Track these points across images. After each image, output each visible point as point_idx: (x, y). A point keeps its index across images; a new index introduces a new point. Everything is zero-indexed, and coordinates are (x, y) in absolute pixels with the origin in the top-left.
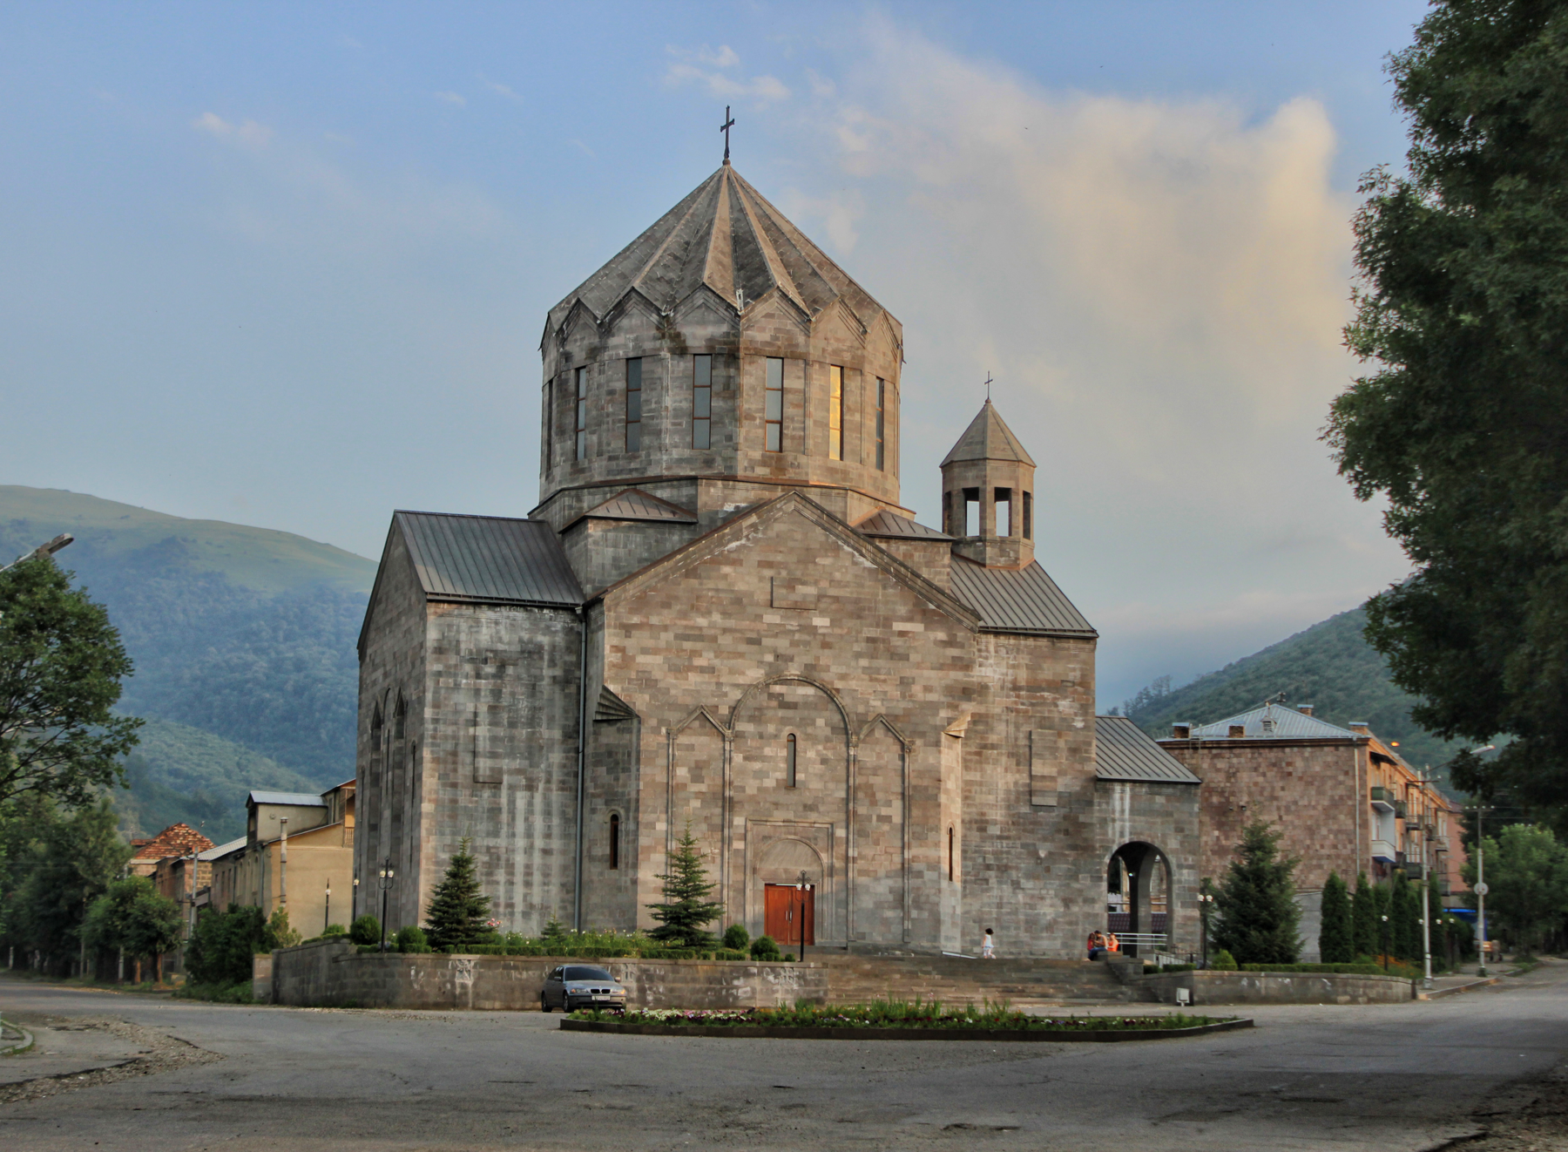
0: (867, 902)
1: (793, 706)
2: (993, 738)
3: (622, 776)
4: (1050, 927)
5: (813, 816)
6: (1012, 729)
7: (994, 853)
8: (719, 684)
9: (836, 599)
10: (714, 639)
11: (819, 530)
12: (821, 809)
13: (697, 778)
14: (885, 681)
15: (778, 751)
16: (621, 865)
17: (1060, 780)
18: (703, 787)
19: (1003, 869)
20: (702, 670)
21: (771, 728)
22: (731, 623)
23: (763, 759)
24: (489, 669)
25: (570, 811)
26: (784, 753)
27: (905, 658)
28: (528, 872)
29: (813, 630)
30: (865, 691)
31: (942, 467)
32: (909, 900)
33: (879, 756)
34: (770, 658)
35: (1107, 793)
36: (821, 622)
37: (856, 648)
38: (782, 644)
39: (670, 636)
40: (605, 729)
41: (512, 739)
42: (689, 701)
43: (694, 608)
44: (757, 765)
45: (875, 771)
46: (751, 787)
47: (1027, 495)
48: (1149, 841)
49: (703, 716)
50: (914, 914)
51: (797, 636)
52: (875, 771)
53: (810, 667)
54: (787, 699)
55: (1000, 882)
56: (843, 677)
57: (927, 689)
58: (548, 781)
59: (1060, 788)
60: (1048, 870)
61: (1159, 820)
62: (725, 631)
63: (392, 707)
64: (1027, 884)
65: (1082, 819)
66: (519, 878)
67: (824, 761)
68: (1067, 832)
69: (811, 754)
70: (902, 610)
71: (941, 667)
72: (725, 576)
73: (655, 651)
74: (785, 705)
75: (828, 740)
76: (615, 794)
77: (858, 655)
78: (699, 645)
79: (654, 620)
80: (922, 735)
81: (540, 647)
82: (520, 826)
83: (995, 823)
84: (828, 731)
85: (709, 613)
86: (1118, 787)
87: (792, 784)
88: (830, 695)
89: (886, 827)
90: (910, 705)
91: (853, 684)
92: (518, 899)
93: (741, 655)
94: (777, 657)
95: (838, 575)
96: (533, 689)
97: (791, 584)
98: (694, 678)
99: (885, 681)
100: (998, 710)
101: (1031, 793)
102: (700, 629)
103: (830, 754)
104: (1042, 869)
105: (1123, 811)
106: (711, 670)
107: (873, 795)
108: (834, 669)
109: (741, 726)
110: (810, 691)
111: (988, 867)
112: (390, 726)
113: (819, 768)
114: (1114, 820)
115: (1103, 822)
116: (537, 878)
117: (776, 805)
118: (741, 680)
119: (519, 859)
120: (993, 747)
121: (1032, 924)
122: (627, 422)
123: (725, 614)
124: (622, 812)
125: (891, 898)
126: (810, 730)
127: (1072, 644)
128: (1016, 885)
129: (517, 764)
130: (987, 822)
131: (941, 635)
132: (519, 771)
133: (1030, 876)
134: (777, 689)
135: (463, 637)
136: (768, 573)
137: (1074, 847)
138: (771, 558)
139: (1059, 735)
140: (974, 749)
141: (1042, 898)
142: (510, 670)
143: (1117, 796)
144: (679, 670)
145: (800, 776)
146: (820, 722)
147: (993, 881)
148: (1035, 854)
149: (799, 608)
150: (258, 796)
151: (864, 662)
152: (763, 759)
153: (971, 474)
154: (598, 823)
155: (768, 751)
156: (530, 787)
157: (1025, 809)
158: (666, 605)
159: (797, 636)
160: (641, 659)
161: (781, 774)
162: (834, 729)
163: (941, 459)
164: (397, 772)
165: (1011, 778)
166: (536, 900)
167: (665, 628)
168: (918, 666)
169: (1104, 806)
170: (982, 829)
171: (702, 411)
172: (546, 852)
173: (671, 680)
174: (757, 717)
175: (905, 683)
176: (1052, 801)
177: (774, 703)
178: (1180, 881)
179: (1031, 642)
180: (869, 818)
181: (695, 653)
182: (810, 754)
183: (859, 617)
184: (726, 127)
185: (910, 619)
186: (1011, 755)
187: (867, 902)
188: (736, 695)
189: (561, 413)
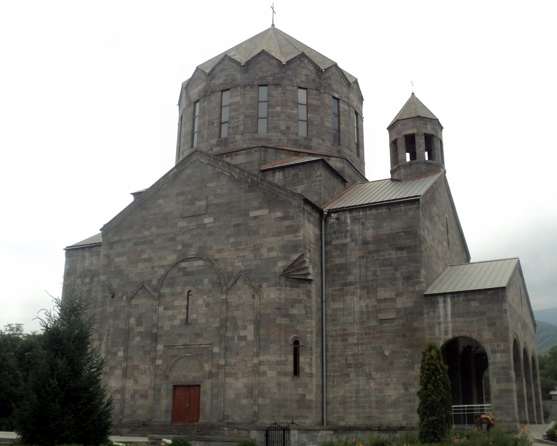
2: (351, 278)
4: (394, 405)
5: (200, 341)
6: (363, 270)
7: (353, 355)
9: (217, 205)
10: (152, 242)
11: (210, 168)
12: (205, 335)
13: (139, 324)
15: (181, 302)
17: (398, 300)
18: (142, 329)
19: (359, 366)
20: (145, 260)
21: (179, 289)
24: (87, 280)
27: (257, 232)
32: (256, 392)
33: (240, 297)
34: (180, 247)
36: (208, 220)
37: (228, 232)
38: (187, 238)
39: (130, 245)
44: (170, 312)
46: (167, 325)
48: (468, 335)
52: (237, 307)
53: (202, 249)
54: (189, 269)
55: (357, 375)
59: (399, 305)
60: (391, 364)
61: (475, 319)
62: (158, 236)
65: (415, 325)
68: (404, 336)
69: (200, 302)
70: (255, 203)
71: (279, 234)
74: (187, 273)
75: (210, 291)
77: (229, 236)
78: (144, 246)
79: (124, 237)
80: (267, 280)
83: (352, 334)
84: (210, 286)
85: (150, 228)
88: (211, 262)
89: (243, 344)
90: (259, 262)
91: (226, 254)
93: (165, 248)
94: (184, 245)
98: (141, 266)
99: (244, 249)
100: (353, 260)
102: (146, 237)
103: (211, 300)
105: (446, 316)
106: (149, 260)
107: (236, 323)
108: (215, 247)
110: (201, 263)
111: (349, 366)
114: (440, 323)
115: (431, 327)
118: (164, 263)
120: (351, 284)
121: (380, 403)
123: (159, 227)
125: (245, 391)
126: (200, 287)
127: (402, 207)
128: (369, 376)
130: (347, 335)
131: (279, 214)
133: (377, 370)
134: (183, 265)
137: (410, 346)
139: (396, 269)
140: (338, 287)
141: (388, 384)
143: (441, 305)
146: (206, 281)
147: (352, 375)
148: (381, 353)
149: (196, 215)
151: (232, 240)
155: (177, 303)
157: (373, 323)
161: (183, 317)
163: (389, 121)
165: (363, 303)
167: (129, 240)
168: (265, 236)
169: (432, 314)
170: (345, 340)
174: (171, 285)
177: (181, 274)
178: (494, 363)
179: (374, 212)
180: (233, 338)
181: (143, 251)
185: (260, 208)
186: (362, 288)
188: (161, 272)
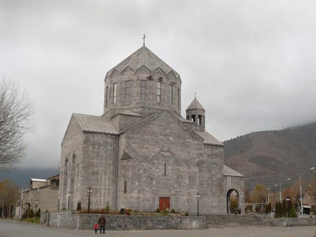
0: (181, 201)
1: (165, 157)
3: (128, 172)
5: (170, 182)
8: (149, 151)
9: (174, 133)
14: (184, 152)
16: (127, 192)
18: (145, 175)
20: (146, 148)
22: (152, 138)
23: (159, 169)
24: (97, 147)
25: (114, 180)
26: (163, 167)
27: (189, 147)
28: (105, 194)
29: (169, 140)
30: (182, 155)
31: (186, 111)
32: (190, 201)
33: (184, 169)
34: (160, 146)
35: (227, 179)
36: (171, 138)
38: (163, 143)
40: (124, 161)
41: (101, 163)
42: (143, 155)
43: (144, 134)
44: (158, 170)
45: (183, 172)
47: (204, 117)
49: (146, 158)
50: (191, 204)
51: (166, 141)
54: (164, 155)
56: (176, 151)
57: (193, 154)
58: (109, 173)
60: (215, 195)
63: (71, 157)
64: (211, 198)
66: (102, 195)
67: (172, 169)
71: (196, 149)
72: (151, 127)
73: (135, 143)
76: (126, 176)
77: (179, 146)
78: (145, 142)
79: (135, 136)
81: (108, 142)
82: (103, 184)
84: (173, 163)
86: (228, 177)
87: (165, 174)
88: (174, 155)
91: (178, 153)
92: (102, 200)
94: (162, 146)
95: (175, 128)
96: (106, 151)
97: (165, 130)
98: (144, 150)
101: (211, 178)
104: (214, 195)
106: (147, 148)
109: (154, 161)
110: (169, 154)
112: (70, 161)
113: (171, 171)
116: (107, 195)
117: (162, 179)
118: (154, 151)
119: (103, 191)
122: (126, 94)
123: (151, 136)
124: (128, 180)
129: (102, 169)
132: (103, 171)
134: (162, 153)
135: (91, 139)
136: (160, 127)
138: (160, 123)
142: (101, 147)
144: (142, 148)
145: (167, 173)
146: (171, 161)
149: (166, 135)
150: (33, 180)
152: (159, 169)
153: (193, 112)
154: (121, 184)
156: (105, 175)
158: (138, 133)
159: (166, 141)
160: (132, 145)
161: (163, 172)
162: (174, 162)
164: (73, 171)
166: (106, 200)
167: (138, 138)
171: (143, 92)
172: (109, 189)
173: (139, 150)
175: (189, 153)
176: (215, 180)
180: (181, 182)
181: (145, 144)
182: (169, 168)
183: (179, 137)
184: (145, 37)
185: (190, 139)
187: (181, 201)
188: (153, 154)
189: (110, 94)
